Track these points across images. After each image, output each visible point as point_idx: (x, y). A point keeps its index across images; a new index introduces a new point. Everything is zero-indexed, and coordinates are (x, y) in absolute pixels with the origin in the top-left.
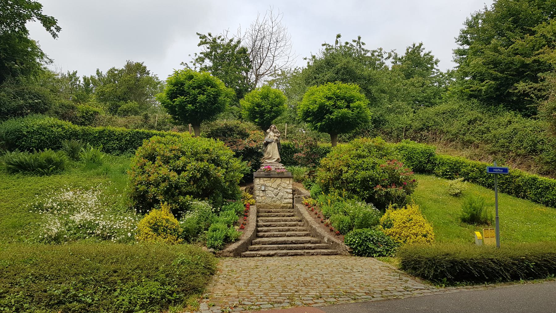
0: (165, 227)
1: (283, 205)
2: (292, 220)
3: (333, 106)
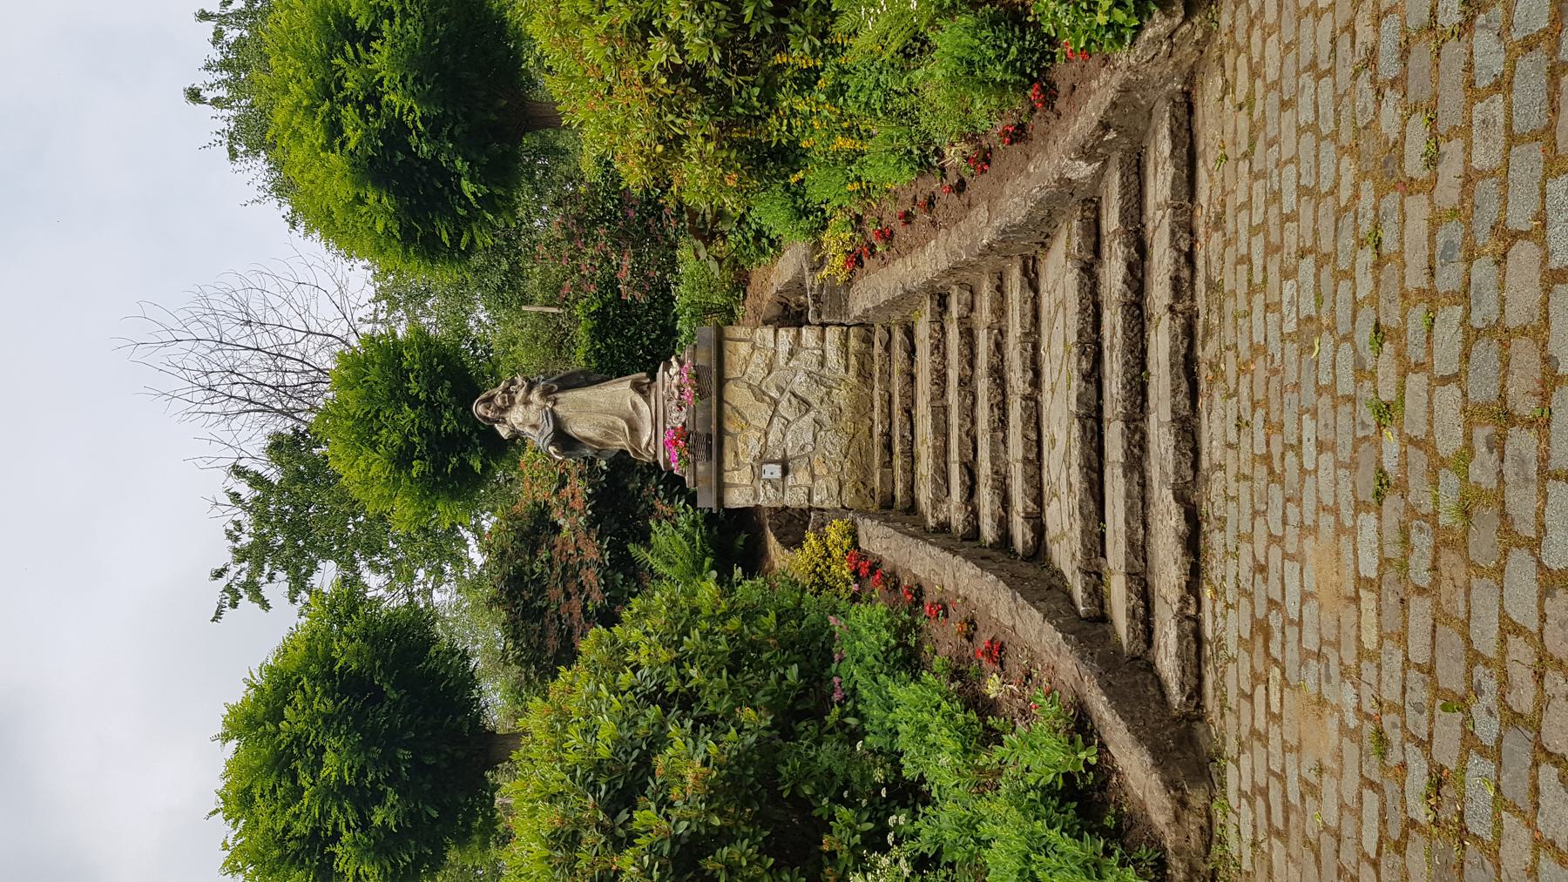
2: (939, 347)
3: (364, 115)
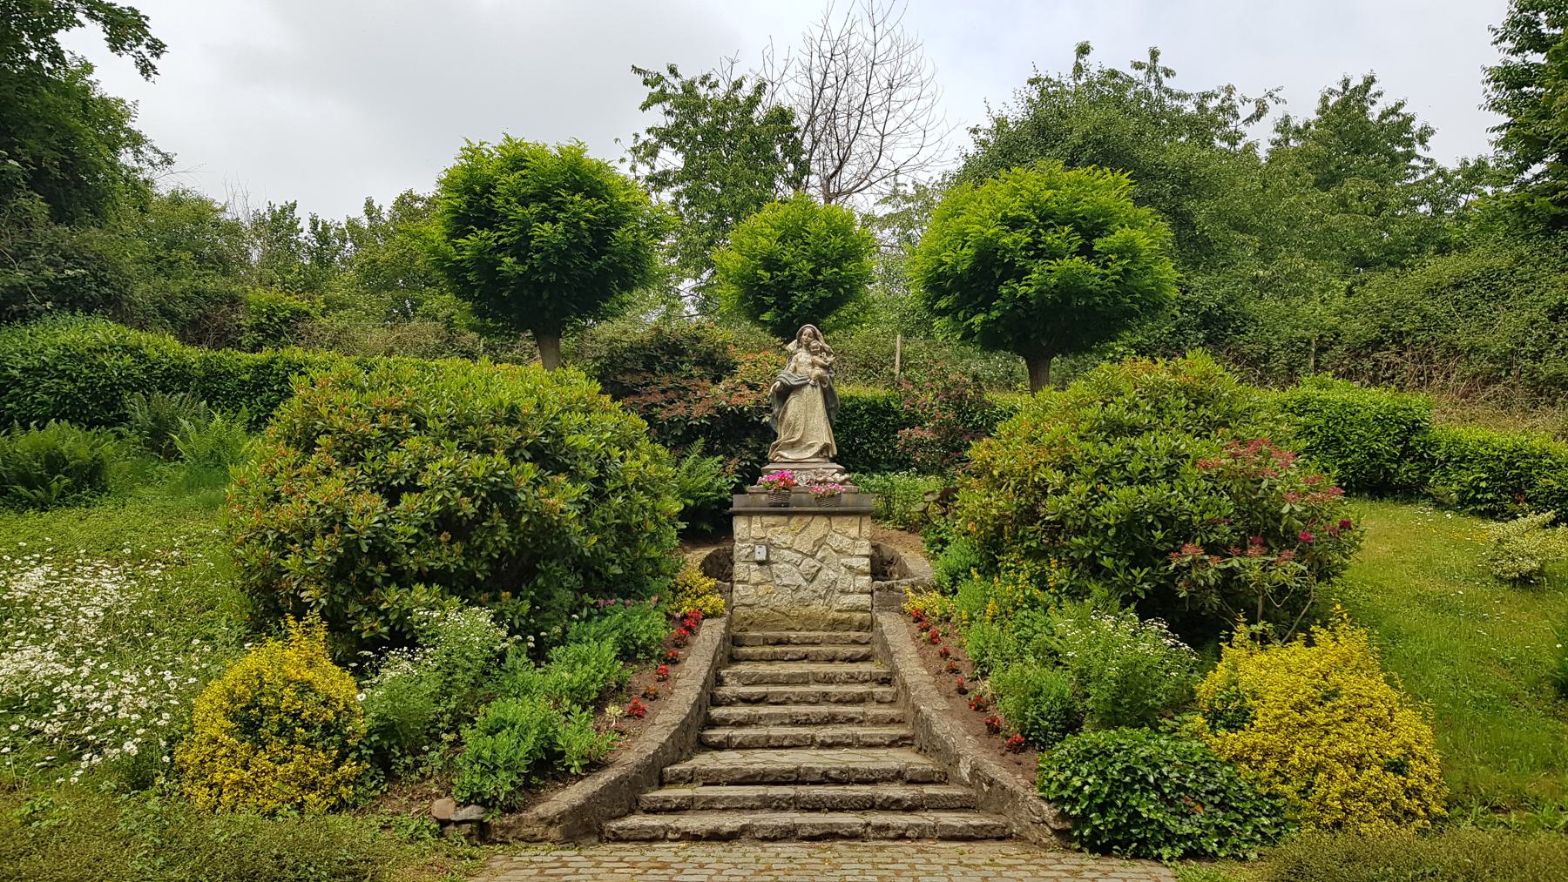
0: (287, 714)
1: (836, 614)
2: (852, 679)
3: (1027, 248)
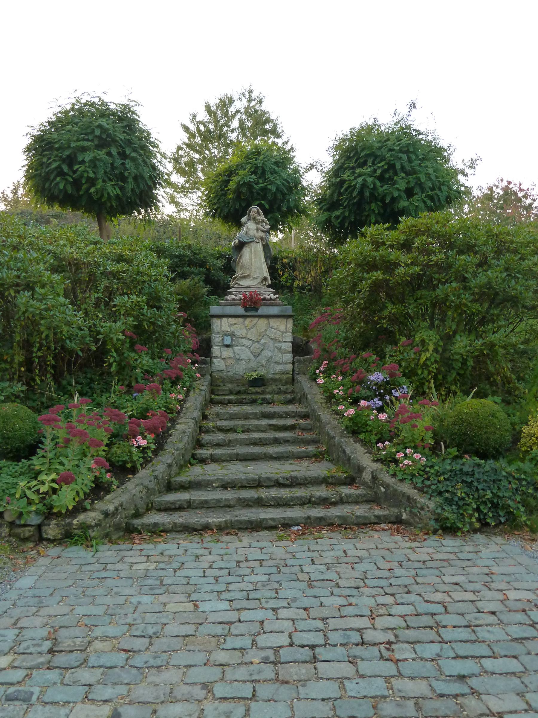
2: (288, 415)
